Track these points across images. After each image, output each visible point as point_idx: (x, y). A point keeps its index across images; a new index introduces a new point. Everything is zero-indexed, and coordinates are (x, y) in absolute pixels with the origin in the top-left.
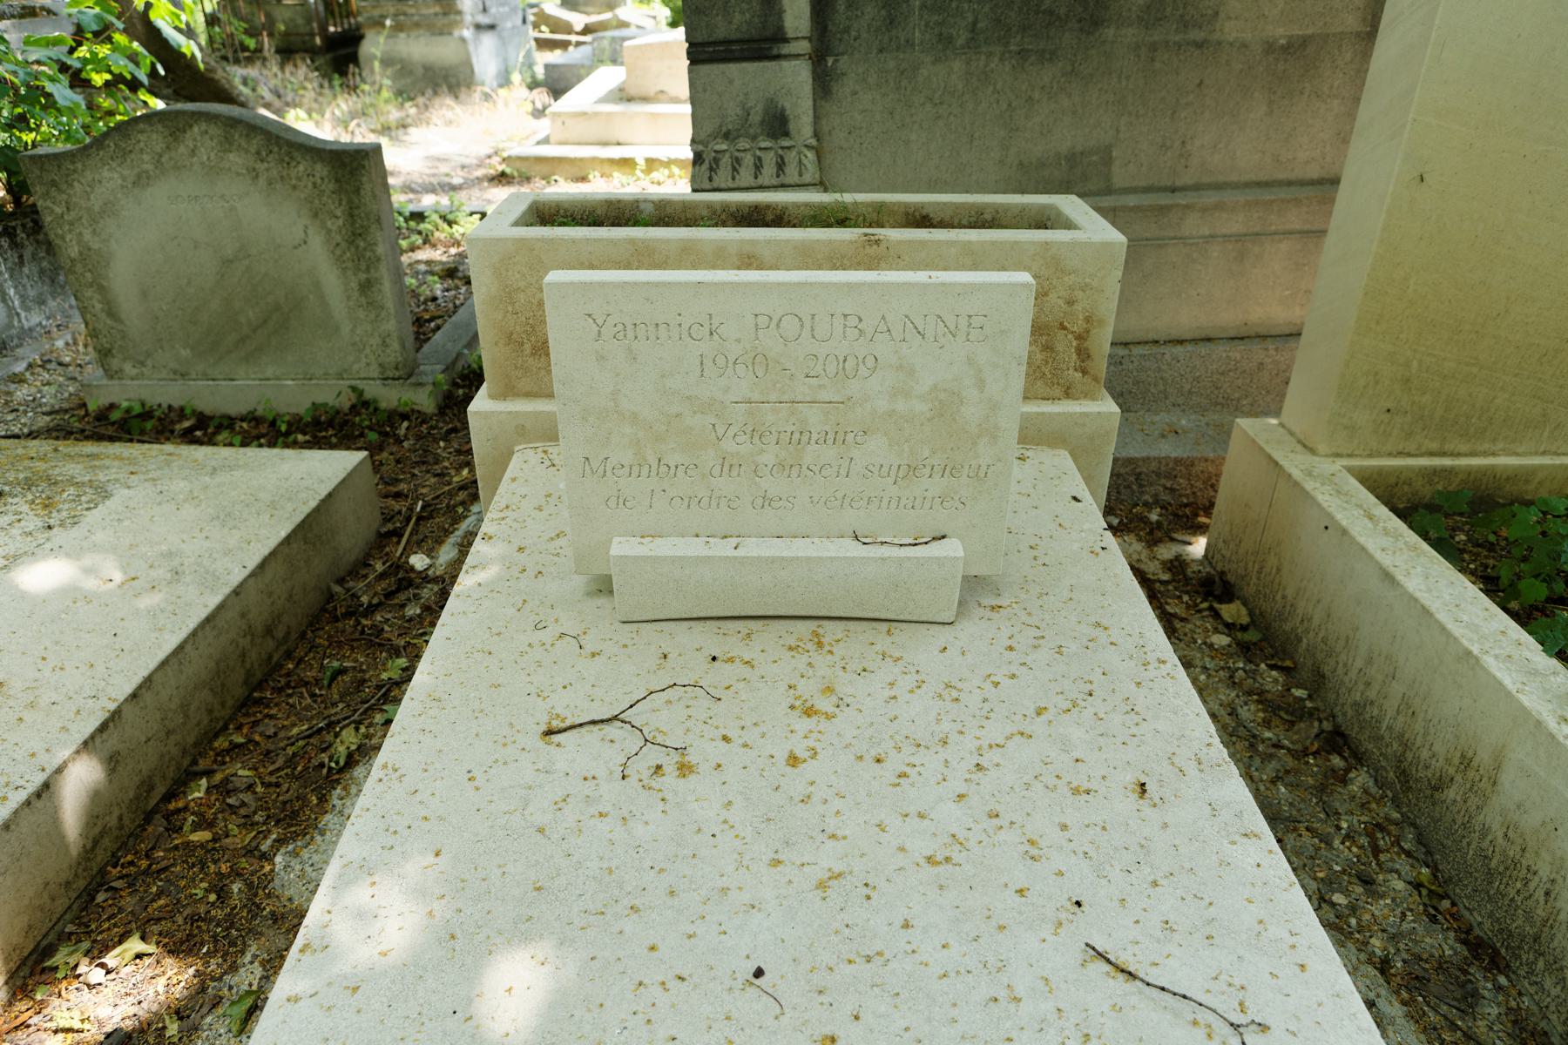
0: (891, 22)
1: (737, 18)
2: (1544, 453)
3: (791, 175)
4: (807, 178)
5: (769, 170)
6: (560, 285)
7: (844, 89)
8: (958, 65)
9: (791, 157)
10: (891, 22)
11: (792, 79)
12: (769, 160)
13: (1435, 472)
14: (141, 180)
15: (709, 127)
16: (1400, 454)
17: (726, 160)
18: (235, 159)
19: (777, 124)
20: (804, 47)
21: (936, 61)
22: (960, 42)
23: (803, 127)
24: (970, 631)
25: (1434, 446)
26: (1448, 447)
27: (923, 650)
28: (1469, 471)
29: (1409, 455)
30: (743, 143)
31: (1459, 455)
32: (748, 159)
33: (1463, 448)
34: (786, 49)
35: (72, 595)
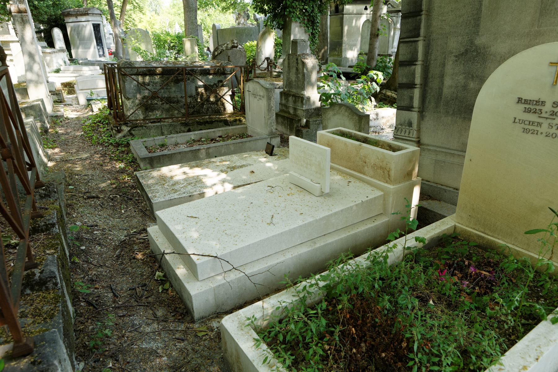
0: (437, 107)
1: (405, 102)
2: (513, 244)
3: (411, 135)
4: (414, 136)
5: (407, 133)
6: (293, 138)
7: (426, 119)
8: (450, 118)
9: (411, 131)
10: (437, 107)
11: (414, 116)
12: (408, 131)
13: (479, 236)
14: (334, 115)
15: (398, 122)
16: (474, 229)
17: (400, 129)
18: (347, 113)
19: (410, 124)
20: (417, 110)
21: (445, 117)
22: (451, 113)
23: (415, 126)
24: (319, 199)
25: (483, 230)
26: (487, 232)
27: (308, 197)
28: (488, 240)
29: (476, 230)
30: (404, 127)
31: (489, 235)
32: (404, 130)
33: (490, 234)
34: (413, 110)
35: (270, 168)
